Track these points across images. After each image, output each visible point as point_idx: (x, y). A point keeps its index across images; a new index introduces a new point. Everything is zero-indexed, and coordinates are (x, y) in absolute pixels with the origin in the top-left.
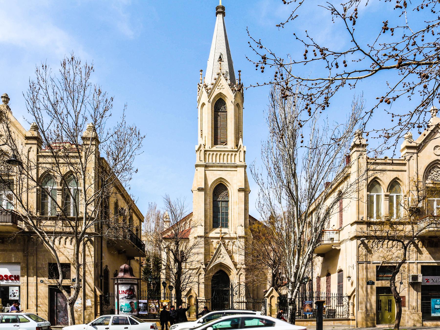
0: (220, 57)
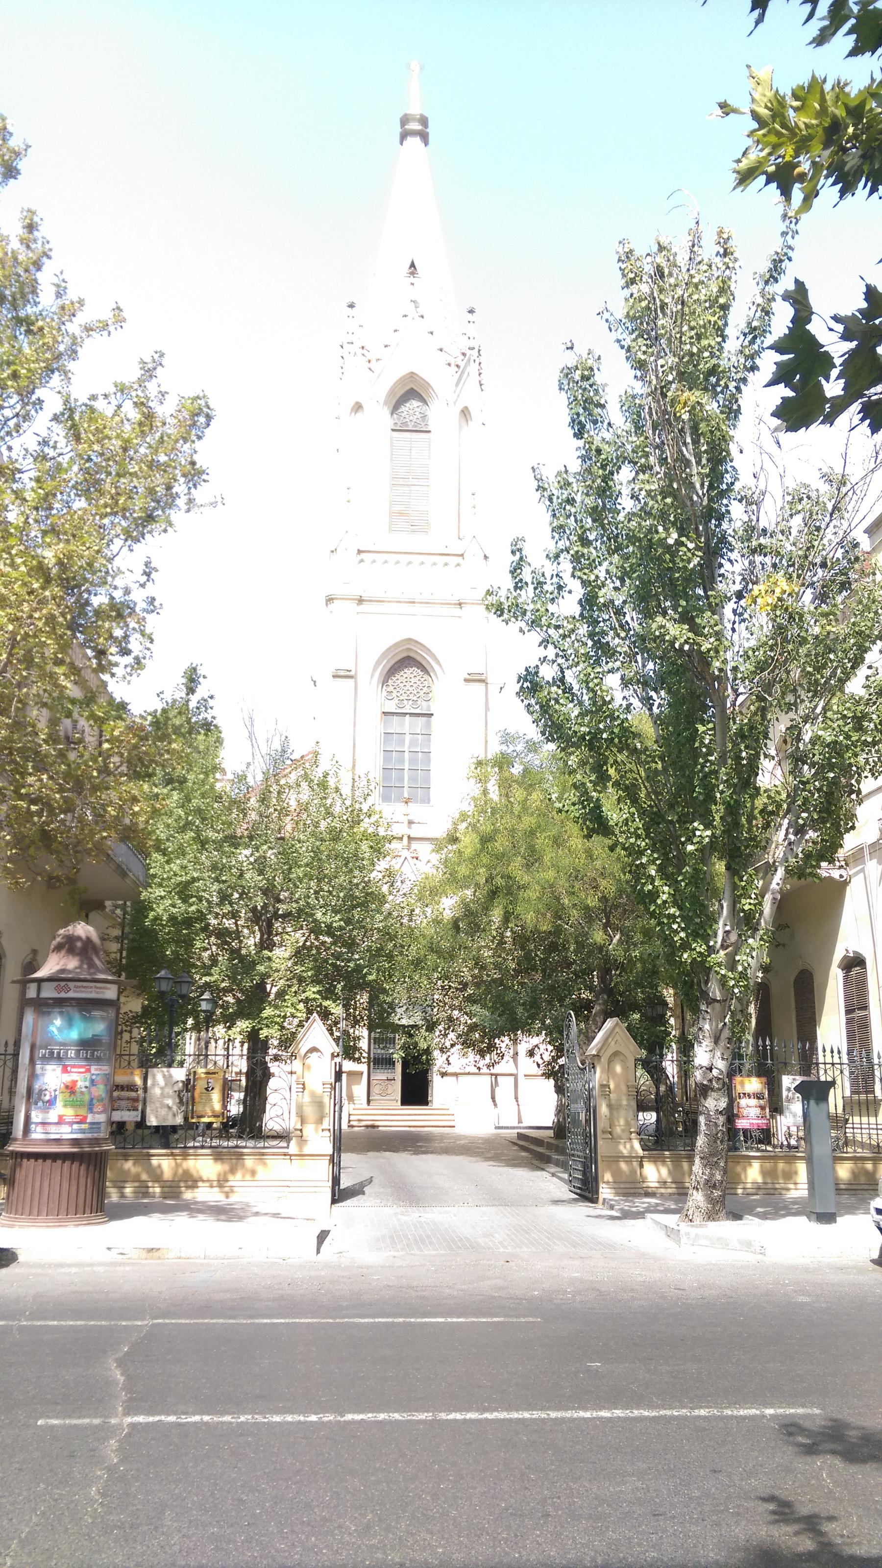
0: (413, 265)
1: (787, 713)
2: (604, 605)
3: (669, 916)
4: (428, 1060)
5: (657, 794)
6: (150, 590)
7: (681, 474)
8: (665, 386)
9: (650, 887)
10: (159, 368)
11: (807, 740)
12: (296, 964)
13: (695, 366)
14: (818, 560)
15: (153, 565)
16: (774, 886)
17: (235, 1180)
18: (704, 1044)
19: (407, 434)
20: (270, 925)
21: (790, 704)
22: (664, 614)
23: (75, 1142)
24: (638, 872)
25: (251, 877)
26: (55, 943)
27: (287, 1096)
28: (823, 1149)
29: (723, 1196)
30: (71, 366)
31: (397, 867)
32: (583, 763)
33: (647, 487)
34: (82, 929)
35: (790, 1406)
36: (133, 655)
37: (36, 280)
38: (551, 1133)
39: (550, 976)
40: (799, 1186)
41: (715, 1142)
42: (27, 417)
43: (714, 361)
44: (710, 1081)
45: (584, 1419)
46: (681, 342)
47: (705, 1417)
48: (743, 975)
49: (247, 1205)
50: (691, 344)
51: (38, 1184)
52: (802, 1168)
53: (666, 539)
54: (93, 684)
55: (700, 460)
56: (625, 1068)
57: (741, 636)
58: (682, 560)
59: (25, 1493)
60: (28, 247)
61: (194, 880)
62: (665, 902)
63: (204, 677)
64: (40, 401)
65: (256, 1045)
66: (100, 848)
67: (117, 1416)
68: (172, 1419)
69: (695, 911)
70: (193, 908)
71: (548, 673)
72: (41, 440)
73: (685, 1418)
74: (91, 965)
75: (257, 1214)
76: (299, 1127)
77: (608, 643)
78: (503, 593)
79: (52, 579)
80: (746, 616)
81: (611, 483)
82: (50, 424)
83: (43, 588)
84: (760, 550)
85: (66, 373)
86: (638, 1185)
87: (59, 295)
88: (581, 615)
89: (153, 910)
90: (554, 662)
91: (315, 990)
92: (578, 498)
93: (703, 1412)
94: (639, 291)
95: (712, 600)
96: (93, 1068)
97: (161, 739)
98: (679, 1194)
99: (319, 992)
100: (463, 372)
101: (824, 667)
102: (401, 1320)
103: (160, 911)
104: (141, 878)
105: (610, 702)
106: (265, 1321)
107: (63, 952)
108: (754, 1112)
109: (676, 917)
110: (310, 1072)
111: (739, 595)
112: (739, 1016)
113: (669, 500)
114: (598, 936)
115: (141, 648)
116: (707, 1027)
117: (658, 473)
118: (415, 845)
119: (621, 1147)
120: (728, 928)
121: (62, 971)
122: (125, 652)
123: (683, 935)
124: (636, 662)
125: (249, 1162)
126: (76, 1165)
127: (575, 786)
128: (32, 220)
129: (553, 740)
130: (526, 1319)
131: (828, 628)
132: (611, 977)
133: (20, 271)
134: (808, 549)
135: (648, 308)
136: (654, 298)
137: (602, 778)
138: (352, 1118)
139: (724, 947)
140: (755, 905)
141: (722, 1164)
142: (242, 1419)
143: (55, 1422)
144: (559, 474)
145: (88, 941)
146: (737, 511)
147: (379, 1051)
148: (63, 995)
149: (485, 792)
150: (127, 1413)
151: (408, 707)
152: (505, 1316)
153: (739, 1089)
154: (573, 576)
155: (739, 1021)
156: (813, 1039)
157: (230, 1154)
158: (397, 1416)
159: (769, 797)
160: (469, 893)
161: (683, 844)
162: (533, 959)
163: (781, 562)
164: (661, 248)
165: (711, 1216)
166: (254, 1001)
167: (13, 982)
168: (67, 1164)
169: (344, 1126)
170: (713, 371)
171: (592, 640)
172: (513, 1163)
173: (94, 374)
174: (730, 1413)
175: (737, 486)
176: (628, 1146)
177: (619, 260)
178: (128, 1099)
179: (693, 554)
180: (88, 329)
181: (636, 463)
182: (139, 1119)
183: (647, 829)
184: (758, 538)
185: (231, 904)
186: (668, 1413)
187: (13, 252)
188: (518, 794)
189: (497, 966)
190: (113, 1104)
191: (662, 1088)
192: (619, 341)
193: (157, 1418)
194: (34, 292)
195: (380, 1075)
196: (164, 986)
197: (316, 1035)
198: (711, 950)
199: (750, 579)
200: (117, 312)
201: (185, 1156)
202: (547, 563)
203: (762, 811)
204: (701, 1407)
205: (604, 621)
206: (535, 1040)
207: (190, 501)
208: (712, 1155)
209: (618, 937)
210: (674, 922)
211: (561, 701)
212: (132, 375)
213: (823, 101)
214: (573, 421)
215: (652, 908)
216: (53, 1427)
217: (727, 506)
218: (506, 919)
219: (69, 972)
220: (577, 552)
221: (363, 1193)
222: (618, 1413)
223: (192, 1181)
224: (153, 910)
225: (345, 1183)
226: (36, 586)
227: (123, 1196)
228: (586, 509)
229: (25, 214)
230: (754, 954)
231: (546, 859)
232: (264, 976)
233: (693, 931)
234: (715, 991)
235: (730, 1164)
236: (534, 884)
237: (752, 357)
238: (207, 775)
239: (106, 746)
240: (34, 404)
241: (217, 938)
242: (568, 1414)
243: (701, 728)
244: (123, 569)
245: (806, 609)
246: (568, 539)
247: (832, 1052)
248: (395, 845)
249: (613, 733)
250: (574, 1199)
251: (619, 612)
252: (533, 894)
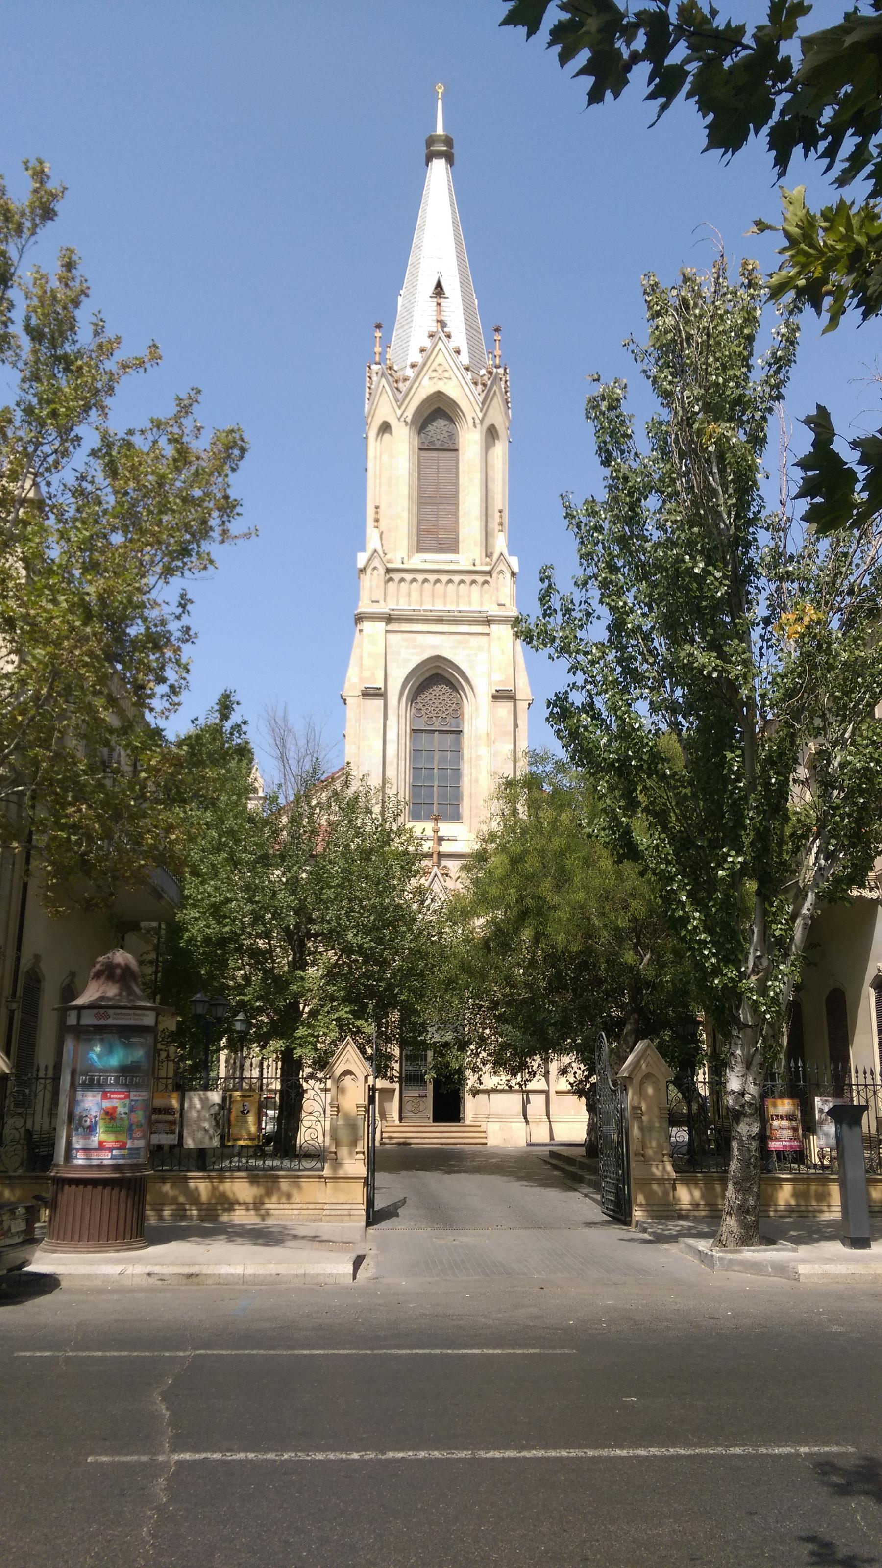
0: (439, 285)
1: (816, 737)
2: (632, 631)
3: (700, 942)
4: (460, 1080)
5: (686, 818)
6: (186, 620)
7: (708, 502)
8: (691, 417)
9: (681, 913)
10: (195, 404)
11: (836, 764)
12: (328, 983)
13: (720, 396)
14: (845, 588)
15: (188, 597)
16: (804, 911)
17: (271, 1204)
18: (737, 1069)
19: (435, 454)
20: (302, 945)
21: (819, 729)
22: (692, 641)
23: (116, 1168)
24: (669, 899)
25: (285, 899)
26: (94, 970)
27: (322, 1119)
28: (856, 1172)
29: (757, 1221)
30: (108, 401)
31: (427, 884)
32: (611, 789)
33: (673, 518)
34: (120, 957)
35: (826, 1443)
36: (168, 683)
37: (74, 318)
38: (582, 1151)
39: (581, 996)
40: (833, 1209)
41: (748, 1167)
42: (65, 453)
43: (740, 391)
44: (743, 1106)
45: (621, 1458)
46: (706, 373)
47: (740, 1456)
48: (775, 1001)
49: (285, 1227)
50: (717, 375)
51: (79, 1209)
52: (835, 1190)
53: (693, 568)
54: (130, 712)
55: (727, 489)
56: (657, 1090)
57: (769, 661)
58: (710, 589)
59: (79, 1534)
60: (67, 285)
61: (229, 901)
62: (695, 928)
63: (238, 703)
64: (78, 438)
65: (290, 1067)
66: (139, 877)
67: (164, 1453)
68: (217, 1456)
69: (726, 936)
70: (227, 929)
71: (578, 698)
72: (79, 475)
73: (721, 1456)
74: (131, 992)
75: (295, 1237)
76: (334, 1150)
77: (636, 668)
78: (532, 620)
79: (93, 616)
80: (774, 641)
81: (638, 510)
82: (87, 459)
83: (85, 624)
84: (788, 576)
85: (103, 408)
86: (671, 1208)
87: (96, 334)
88: (610, 640)
89: (187, 930)
90: (583, 688)
91: (347, 1009)
92: (606, 525)
93: (738, 1451)
94: (664, 322)
95: (739, 627)
96: (132, 1094)
97: (196, 765)
98: (712, 1217)
99: (350, 1012)
100: (489, 391)
101: (852, 691)
102: (438, 1351)
103: (194, 931)
104: (176, 900)
105: (638, 730)
106: (305, 1352)
107: (102, 979)
108: (787, 1134)
109: (706, 943)
110: (343, 1093)
111: (767, 621)
112: (771, 1041)
113: (696, 530)
114: (629, 957)
115: (177, 677)
116: (739, 1052)
117: (685, 501)
118: (444, 863)
119: (654, 1170)
120: (758, 953)
121: (102, 998)
122: (161, 680)
123: (713, 960)
124: (665, 686)
125: (284, 1185)
126: (116, 1191)
127: (604, 810)
128: (70, 258)
129: (583, 765)
130: (562, 1351)
131: (857, 652)
132: (642, 996)
133: (59, 309)
134: (836, 575)
135: (674, 340)
136: (680, 331)
137: (632, 805)
138: (384, 1135)
139: (755, 972)
140: (786, 931)
141: (755, 1189)
142: (286, 1456)
143: (105, 1459)
144: (586, 502)
145: (127, 968)
146: (764, 538)
147: (411, 1068)
148: (103, 1022)
149: (515, 812)
150: (173, 1451)
151: (437, 724)
152: (540, 1347)
153: (772, 1111)
154: (601, 602)
155: (771, 1047)
156: (845, 1059)
157: (265, 1177)
158: (436, 1454)
159: (799, 821)
160: (500, 914)
161: (713, 868)
162: (564, 978)
163: (808, 586)
164: (686, 279)
165: (745, 1241)
166: (286, 1022)
167: (54, 1009)
168: (107, 1191)
169: (377, 1144)
170: (739, 401)
171: (621, 666)
172: (546, 1183)
173: (132, 409)
174: (765, 1451)
175: (763, 515)
176: (660, 1167)
177: (645, 293)
178: (166, 1122)
179: (721, 583)
180: (125, 366)
181: (662, 493)
182: (176, 1142)
183: (676, 853)
184: (785, 565)
185: (264, 925)
186: (704, 1451)
187: (52, 291)
188: (547, 814)
189: (528, 986)
190: (152, 1127)
191: (695, 1107)
192: (645, 371)
193: (203, 1456)
194: (72, 328)
195: (412, 1093)
196: (200, 1009)
197: (350, 1059)
198: (743, 976)
199: (777, 606)
200: (153, 349)
201: (222, 1179)
202: (576, 590)
203: (793, 835)
204: (737, 1445)
205: (632, 646)
206: (566, 1060)
207: (225, 532)
208: (746, 1179)
209: (648, 956)
210: (705, 948)
211: (590, 729)
212: (167, 410)
213: (849, 227)
214: (600, 449)
215: (683, 933)
216: (103, 1464)
217: (754, 533)
218: (537, 938)
219: (109, 999)
220: (605, 578)
221: (397, 1215)
222: (654, 1451)
223: (230, 1204)
224: (187, 930)
225: (379, 1204)
226: (78, 623)
227: (161, 1218)
228: (613, 535)
229: (64, 252)
230: (786, 979)
231: (577, 880)
232: (298, 995)
233: (724, 957)
234: (745, 1015)
235: (763, 1186)
236: (564, 906)
237: (777, 386)
238: (239, 796)
239: (143, 775)
240: (72, 441)
241: (250, 958)
242: (605, 1453)
243: (729, 755)
244: (159, 601)
245: (834, 636)
246: (596, 565)
247: (865, 1073)
248: (425, 862)
249: (641, 759)
250: (607, 1222)
251: (647, 638)
252: (563, 914)
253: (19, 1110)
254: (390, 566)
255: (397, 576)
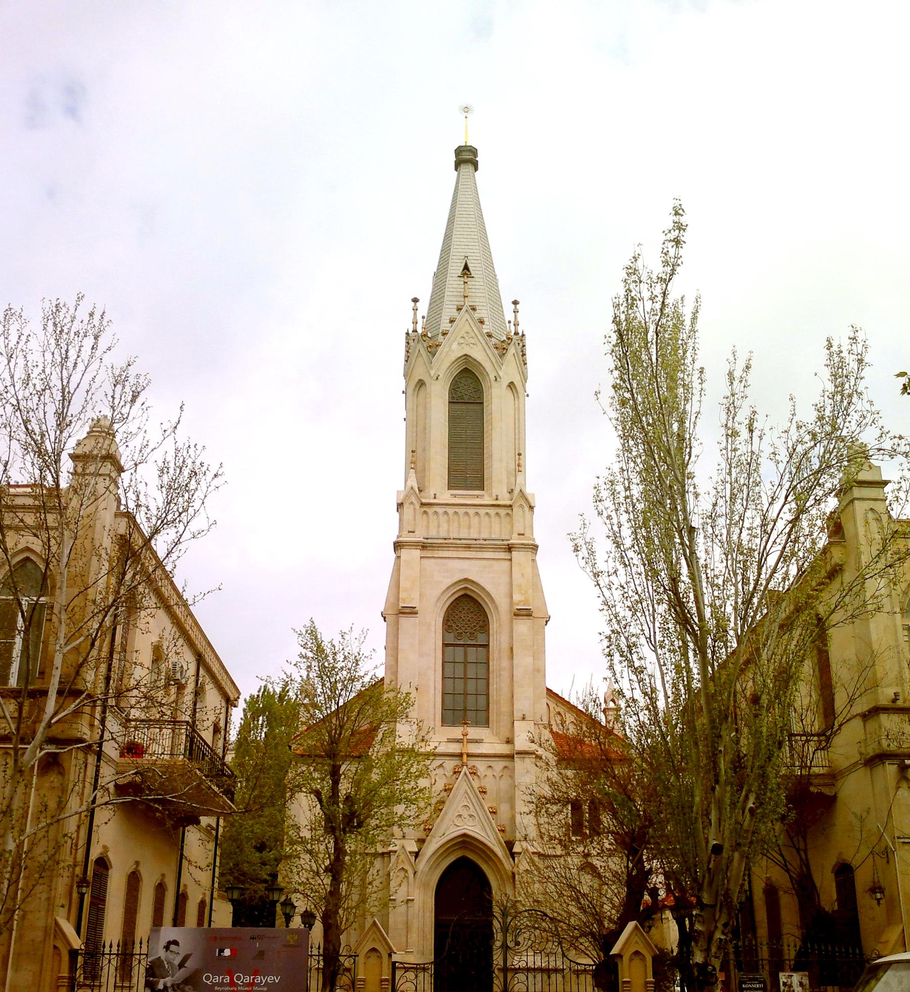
0: (466, 267)
19: (464, 407)
253: (88, 982)
254: (424, 501)
255: (431, 511)
